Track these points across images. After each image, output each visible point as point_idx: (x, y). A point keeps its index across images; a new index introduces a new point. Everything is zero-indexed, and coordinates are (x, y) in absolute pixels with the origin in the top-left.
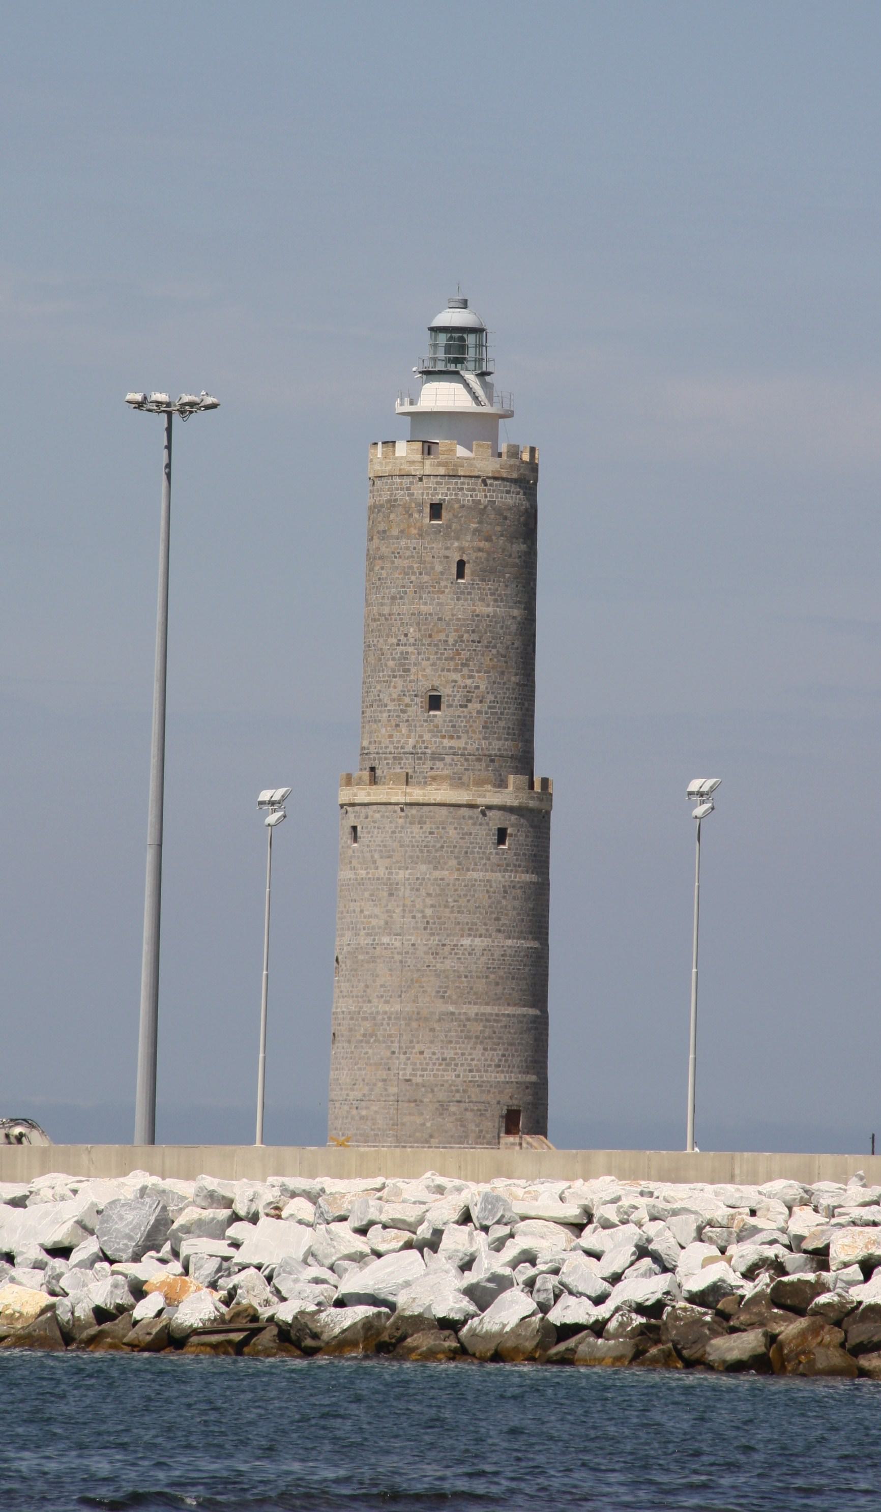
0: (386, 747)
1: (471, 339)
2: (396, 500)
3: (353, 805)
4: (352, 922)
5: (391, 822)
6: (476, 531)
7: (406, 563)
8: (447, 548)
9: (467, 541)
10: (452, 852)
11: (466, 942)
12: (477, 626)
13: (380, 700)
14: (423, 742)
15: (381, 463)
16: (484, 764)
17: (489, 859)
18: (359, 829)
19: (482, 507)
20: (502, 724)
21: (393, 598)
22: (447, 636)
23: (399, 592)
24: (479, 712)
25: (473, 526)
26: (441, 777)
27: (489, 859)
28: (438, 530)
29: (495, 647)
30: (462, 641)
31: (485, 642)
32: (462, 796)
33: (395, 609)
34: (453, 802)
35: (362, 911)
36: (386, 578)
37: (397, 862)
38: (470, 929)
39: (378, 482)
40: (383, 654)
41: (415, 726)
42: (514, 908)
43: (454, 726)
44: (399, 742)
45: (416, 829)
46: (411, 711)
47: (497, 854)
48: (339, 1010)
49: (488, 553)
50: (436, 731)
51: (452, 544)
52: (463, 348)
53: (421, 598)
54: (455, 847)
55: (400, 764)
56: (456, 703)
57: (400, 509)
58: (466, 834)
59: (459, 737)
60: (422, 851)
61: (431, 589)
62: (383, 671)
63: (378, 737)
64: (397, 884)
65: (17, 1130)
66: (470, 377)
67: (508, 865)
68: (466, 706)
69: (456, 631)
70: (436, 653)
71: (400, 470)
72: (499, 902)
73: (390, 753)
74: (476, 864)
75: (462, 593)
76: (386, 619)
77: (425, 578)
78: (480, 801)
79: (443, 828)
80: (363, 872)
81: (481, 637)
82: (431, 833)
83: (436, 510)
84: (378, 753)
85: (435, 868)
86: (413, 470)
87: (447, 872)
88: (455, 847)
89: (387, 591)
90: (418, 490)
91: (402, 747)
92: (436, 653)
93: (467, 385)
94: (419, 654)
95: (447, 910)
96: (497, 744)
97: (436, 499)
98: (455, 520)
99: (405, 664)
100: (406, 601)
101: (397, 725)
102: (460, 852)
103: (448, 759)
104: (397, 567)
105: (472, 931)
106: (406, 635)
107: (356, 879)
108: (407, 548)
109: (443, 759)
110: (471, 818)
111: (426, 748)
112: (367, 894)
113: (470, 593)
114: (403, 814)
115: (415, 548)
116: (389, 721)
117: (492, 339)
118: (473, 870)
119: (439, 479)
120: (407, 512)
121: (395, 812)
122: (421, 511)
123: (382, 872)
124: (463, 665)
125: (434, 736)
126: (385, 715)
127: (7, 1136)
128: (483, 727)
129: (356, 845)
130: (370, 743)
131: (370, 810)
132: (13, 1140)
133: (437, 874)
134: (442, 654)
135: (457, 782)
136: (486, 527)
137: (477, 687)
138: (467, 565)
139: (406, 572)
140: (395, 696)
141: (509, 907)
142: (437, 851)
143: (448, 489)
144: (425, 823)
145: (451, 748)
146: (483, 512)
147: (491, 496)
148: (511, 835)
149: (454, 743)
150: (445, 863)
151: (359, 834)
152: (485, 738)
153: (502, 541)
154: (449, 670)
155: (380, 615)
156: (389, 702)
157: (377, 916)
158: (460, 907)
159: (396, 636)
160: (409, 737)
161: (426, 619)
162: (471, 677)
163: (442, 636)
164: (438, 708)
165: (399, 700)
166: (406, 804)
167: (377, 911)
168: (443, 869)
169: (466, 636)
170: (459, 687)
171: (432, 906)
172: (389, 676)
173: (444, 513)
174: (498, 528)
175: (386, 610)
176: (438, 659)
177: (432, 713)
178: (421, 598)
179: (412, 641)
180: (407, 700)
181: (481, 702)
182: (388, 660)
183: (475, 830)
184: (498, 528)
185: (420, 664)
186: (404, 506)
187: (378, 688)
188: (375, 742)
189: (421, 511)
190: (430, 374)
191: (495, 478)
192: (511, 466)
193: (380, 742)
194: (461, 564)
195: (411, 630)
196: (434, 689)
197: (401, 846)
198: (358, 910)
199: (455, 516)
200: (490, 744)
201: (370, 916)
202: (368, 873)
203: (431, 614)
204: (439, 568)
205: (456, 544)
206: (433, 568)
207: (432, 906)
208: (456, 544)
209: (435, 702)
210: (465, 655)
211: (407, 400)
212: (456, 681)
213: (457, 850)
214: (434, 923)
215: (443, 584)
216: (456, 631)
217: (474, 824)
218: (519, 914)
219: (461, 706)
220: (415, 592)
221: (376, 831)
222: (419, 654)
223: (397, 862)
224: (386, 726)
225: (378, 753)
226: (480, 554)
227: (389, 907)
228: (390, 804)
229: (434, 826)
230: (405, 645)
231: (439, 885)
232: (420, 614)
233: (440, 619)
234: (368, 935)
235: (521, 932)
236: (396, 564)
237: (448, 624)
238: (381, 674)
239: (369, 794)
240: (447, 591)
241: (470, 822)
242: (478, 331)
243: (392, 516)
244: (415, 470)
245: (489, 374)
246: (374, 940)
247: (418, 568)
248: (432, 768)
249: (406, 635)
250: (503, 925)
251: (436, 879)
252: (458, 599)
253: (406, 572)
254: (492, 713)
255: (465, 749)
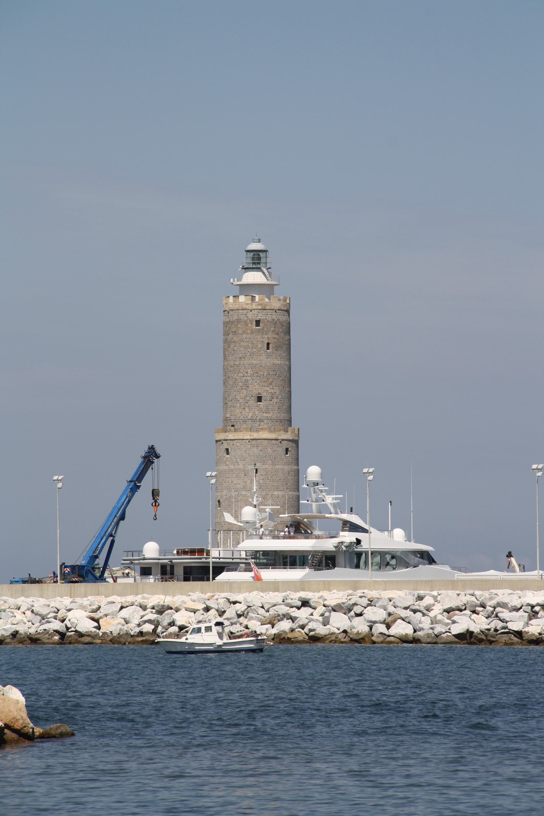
0: (239, 417)
1: (261, 254)
2: (240, 319)
3: (226, 440)
4: (227, 486)
5: (244, 447)
6: (273, 331)
7: (246, 344)
8: (263, 338)
9: (270, 335)
10: (270, 458)
11: (276, 493)
12: (275, 369)
13: (236, 399)
14: (255, 415)
15: (232, 305)
16: (279, 423)
17: (283, 460)
18: (230, 449)
19: (275, 321)
20: (284, 407)
21: (241, 358)
22: (264, 373)
23: (243, 356)
24: (276, 403)
25: (272, 329)
26: (264, 428)
27: (283, 460)
28: (259, 331)
29: (281, 377)
30: (269, 375)
31: (277, 375)
32: (273, 436)
33: (242, 362)
34: (270, 438)
35: (232, 482)
36: (237, 350)
37: (248, 462)
38: (277, 488)
39: (231, 312)
40: (236, 380)
41: (252, 408)
42: (292, 480)
43: (267, 408)
44: (245, 415)
45: (255, 449)
46: (250, 403)
47: (286, 458)
48: (222, 521)
49: (278, 340)
50: (260, 410)
51: (265, 336)
52: (259, 259)
53: (253, 358)
54: (271, 456)
55: (246, 423)
56: (268, 399)
57: (243, 323)
58: (275, 451)
59: (269, 413)
60: (258, 458)
61: (257, 354)
62: (237, 387)
63: (235, 413)
64: (248, 471)
65: (127, 571)
66: (265, 270)
67: (289, 463)
68: (272, 400)
69: (267, 371)
70: (260, 380)
71: (242, 307)
72: (287, 477)
73: (241, 419)
74: (278, 463)
75: (269, 356)
76: (238, 366)
77: (254, 350)
78: (279, 438)
79: (266, 449)
80: (232, 467)
81: (276, 373)
82: (261, 451)
83: (258, 323)
84: (235, 419)
85: (263, 464)
86: (247, 307)
87: (267, 466)
88: (271, 456)
89: (238, 355)
90: (250, 315)
91: (247, 417)
92: (260, 380)
93: (264, 273)
94: (253, 380)
95: (269, 481)
96: (283, 415)
97: (258, 319)
98: (265, 327)
99: (247, 384)
100: (246, 359)
101: (244, 408)
102: (273, 458)
103: (265, 421)
104: (242, 346)
105: (278, 489)
106: (247, 373)
107: (229, 469)
108: (246, 338)
109: (264, 421)
110: (276, 444)
111: (257, 417)
112: (234, 475)
113: (272, 356)
114: (249, 443)
115: (249, 338)
116: (240, 407)
117: (269, 254)
118: (278, 465)
119: (258, 311)
120: (246, 324)
121: (246, 442)
122: (252, 323)
123: (241, 466)
124: (270, 384)
125: (259, 412)
126: (238, 404)
127: (123, 573)
128: (278, 409)
129: (228, 456)
130: (231, 415)
131: (235, 442)
132: (125, 575)
133: (264, 467)
134: (262, 380)
135: (270, 431)
136: (277, 330)
137: (275, 393)
138: (270, 345)
139: (246, 348)
140: (243, 397)
141: (290, 479)
142: (264, 458)
143: (263, 314)
144: (259, 447)
145: (266, 417)
146: (275, 323)
147: (278, 317)
148: (290, 451)
149: (267, 415)
150: (267, 462)
151: (230, 451)
152: (279, 413)
153: (282, 334)
154: (265, 386)
155: (234, 365)
156: (240, 399)
157: (239, 484)
158: (273, 479)
159: (242, 373)
160: (249, 413)
161: (255, 366)
162: (273, 389)
163: (262, 373)
164: (261, 401)
165: (245, 398)
166: (251, 439)
167: (239, 482)
168: (266, 465)
169: (271, 373)
170: (269, 393)
171: (263, 479)
172: (240, 389)
173: (261, 324)
174: (281, 330)
175: (237, 363)
176: (260, 382)
177: (258, 403)
178: (253, 358)
179: (249, 375)
180: (248, 398)
181: (277, 398)
182: (239, 382)
183: (277, 449)
184: (281, 330)
185: (253, 384)
186: (244, 321)
187: (235, 393)
188: (234, 415)
189: (252, 323)
190: (246, 269)
191: (279, 310)
192: (284, 305)
193: (236, 415)
194: (268, 344)
195: (249, 371)
196: (259, 394)
197: (249, 456)
198: (230, 482)
199: (265, 325)
200: (280, 415)
201: (236, 484)
202: (234, 467)
203: (257, 364)
204: (260, 346)
205: (266, 336)
206: (257, 346)
207: (263, 479)
208: (266, 336)
209: (259, 399)
210: (271, 380)
211: (236, 279)
212: (267, 391)
213: (271, 457)
214: (264, 486)
215: (261, 352)
216: (267, 371)
217: (278, 447)
218: (293, 482)
219: (270, 400)
220: (250, 355)
221: (238, 450)
222: (253, 380)
223: (248, 462)
224: (239, 409)
225: (235, 419)
226: (275, 340)
227: (245, 480)
228: (244, 439)
229: (262, 448)
230: (247, 376)
231: (265, 471)
232: (252, 364)
233: (261, 366)
234: (235, 491)
235: (294, 489)
236: (241, 344)
237: (264, 368)
238: (236, 388)
239: (234, 436)
240: (263, 355)
241: (276, 446)
242: (265, 251)
243: (239, 326)
244: (248, 307)
245: (270, 268)
246: (239, 493)
247: (251, 346)
248: (259, 425)
249: (247, 373)
250: (289, 486)
251: (264, 469)
252: (267, 358)
253: (246, 348)
254: (281, 403)
255: (272, 417)
